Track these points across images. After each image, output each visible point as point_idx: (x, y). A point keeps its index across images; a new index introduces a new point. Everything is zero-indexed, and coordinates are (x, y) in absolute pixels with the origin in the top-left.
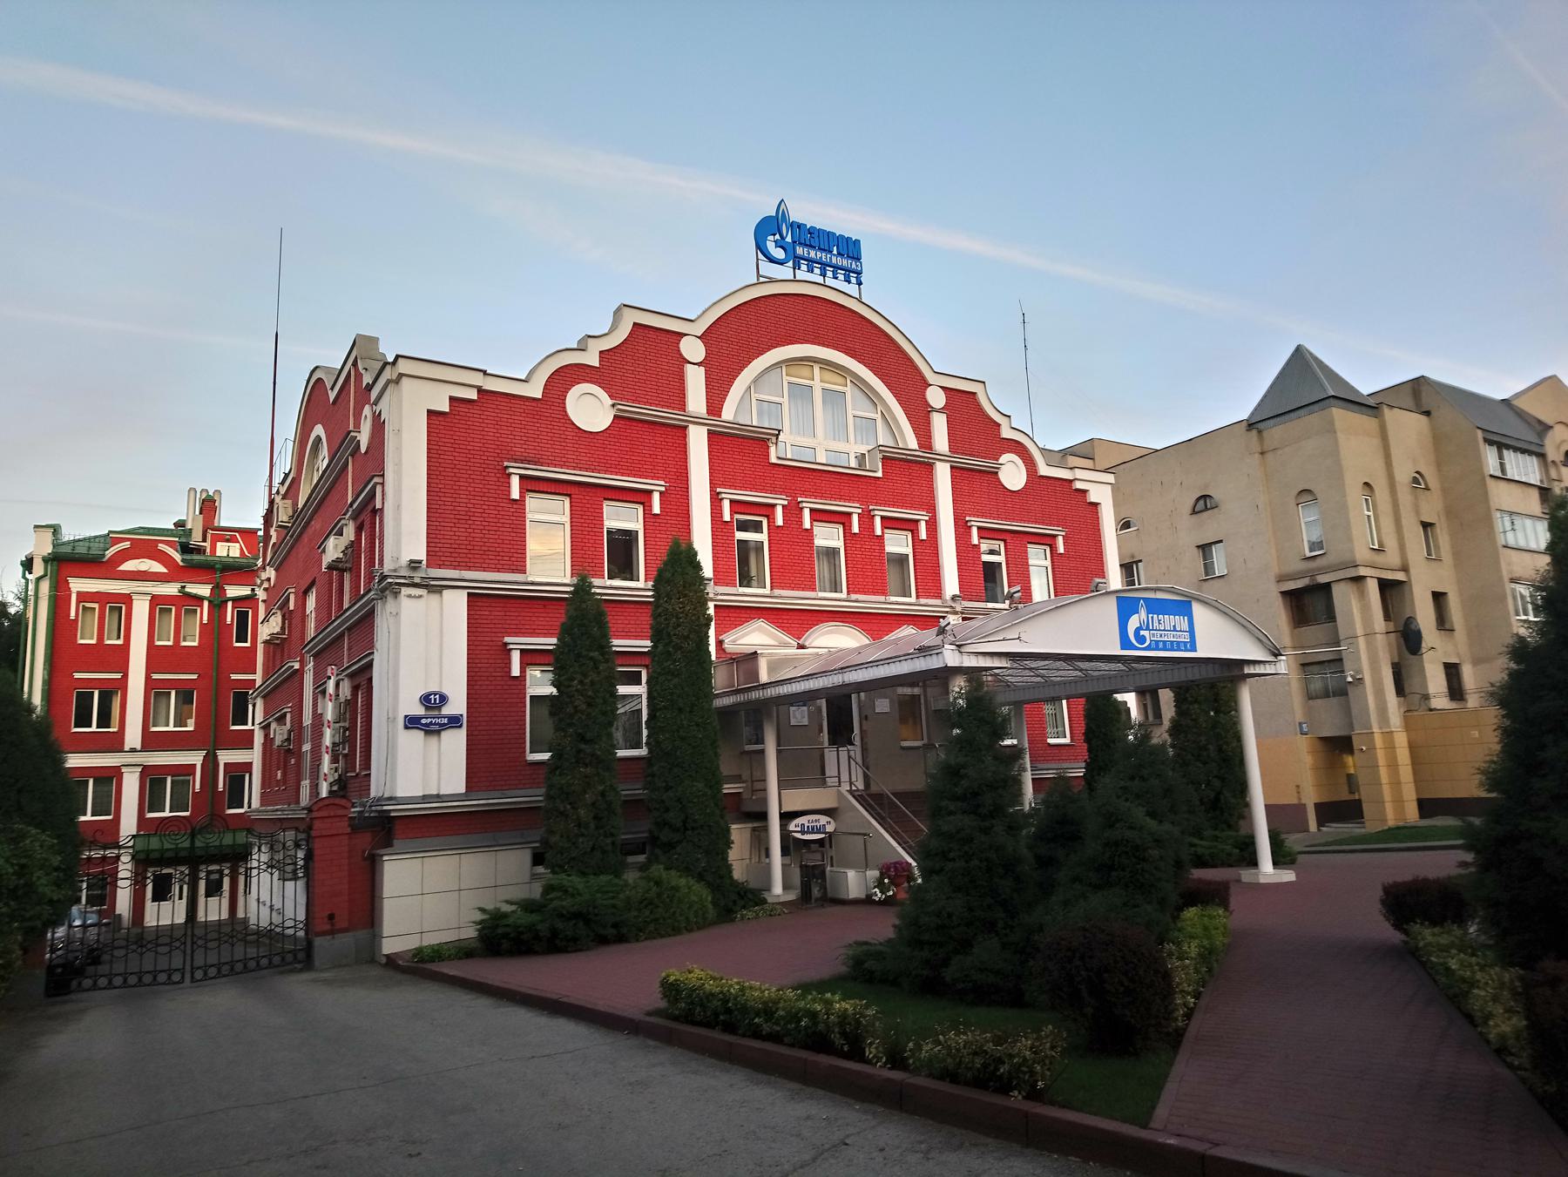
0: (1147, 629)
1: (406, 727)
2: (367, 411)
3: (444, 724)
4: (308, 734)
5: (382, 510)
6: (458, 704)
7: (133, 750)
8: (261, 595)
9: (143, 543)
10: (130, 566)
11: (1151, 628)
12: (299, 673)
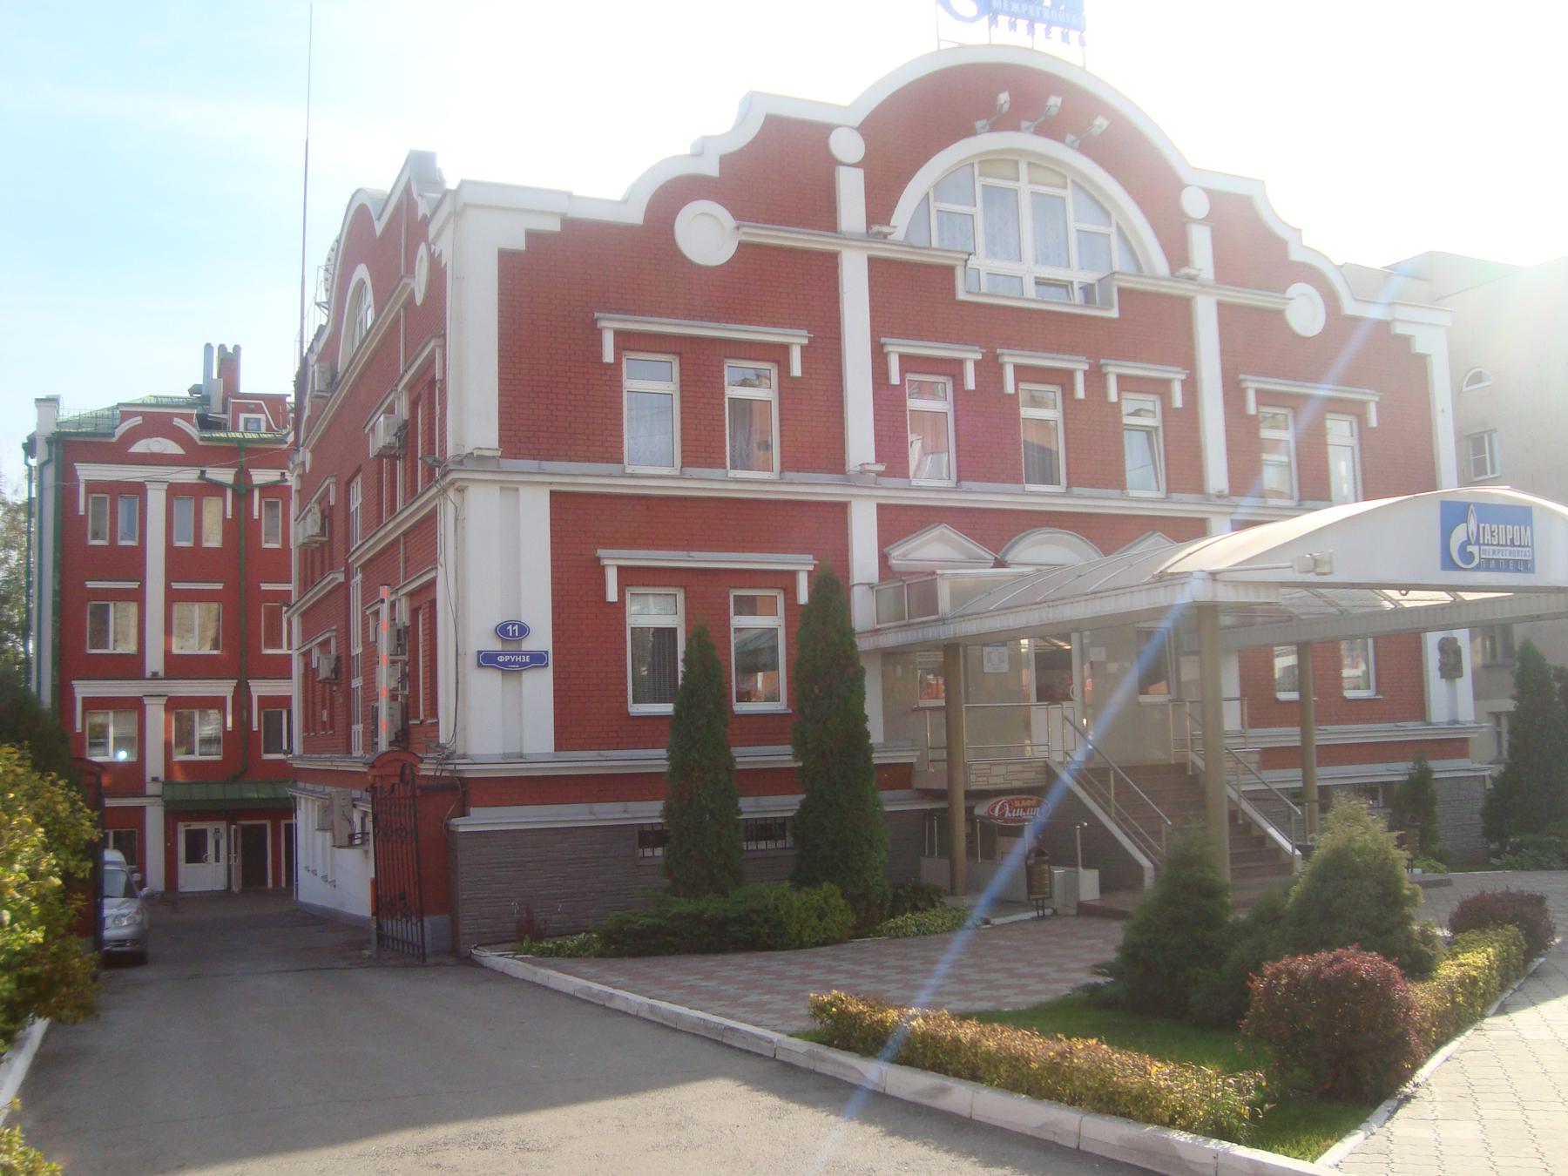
0: (1477, 543)
1: (479, 665)
2: (422, 251)
3: (525, 664)
4: (358, 666)
5: (443, 381)
6: (541, 638)
7: (155, 676)
8: (292, 481)
9: (156, 419)
10: (140, 447)
11: (1481, 542)
12: (345, 587)
